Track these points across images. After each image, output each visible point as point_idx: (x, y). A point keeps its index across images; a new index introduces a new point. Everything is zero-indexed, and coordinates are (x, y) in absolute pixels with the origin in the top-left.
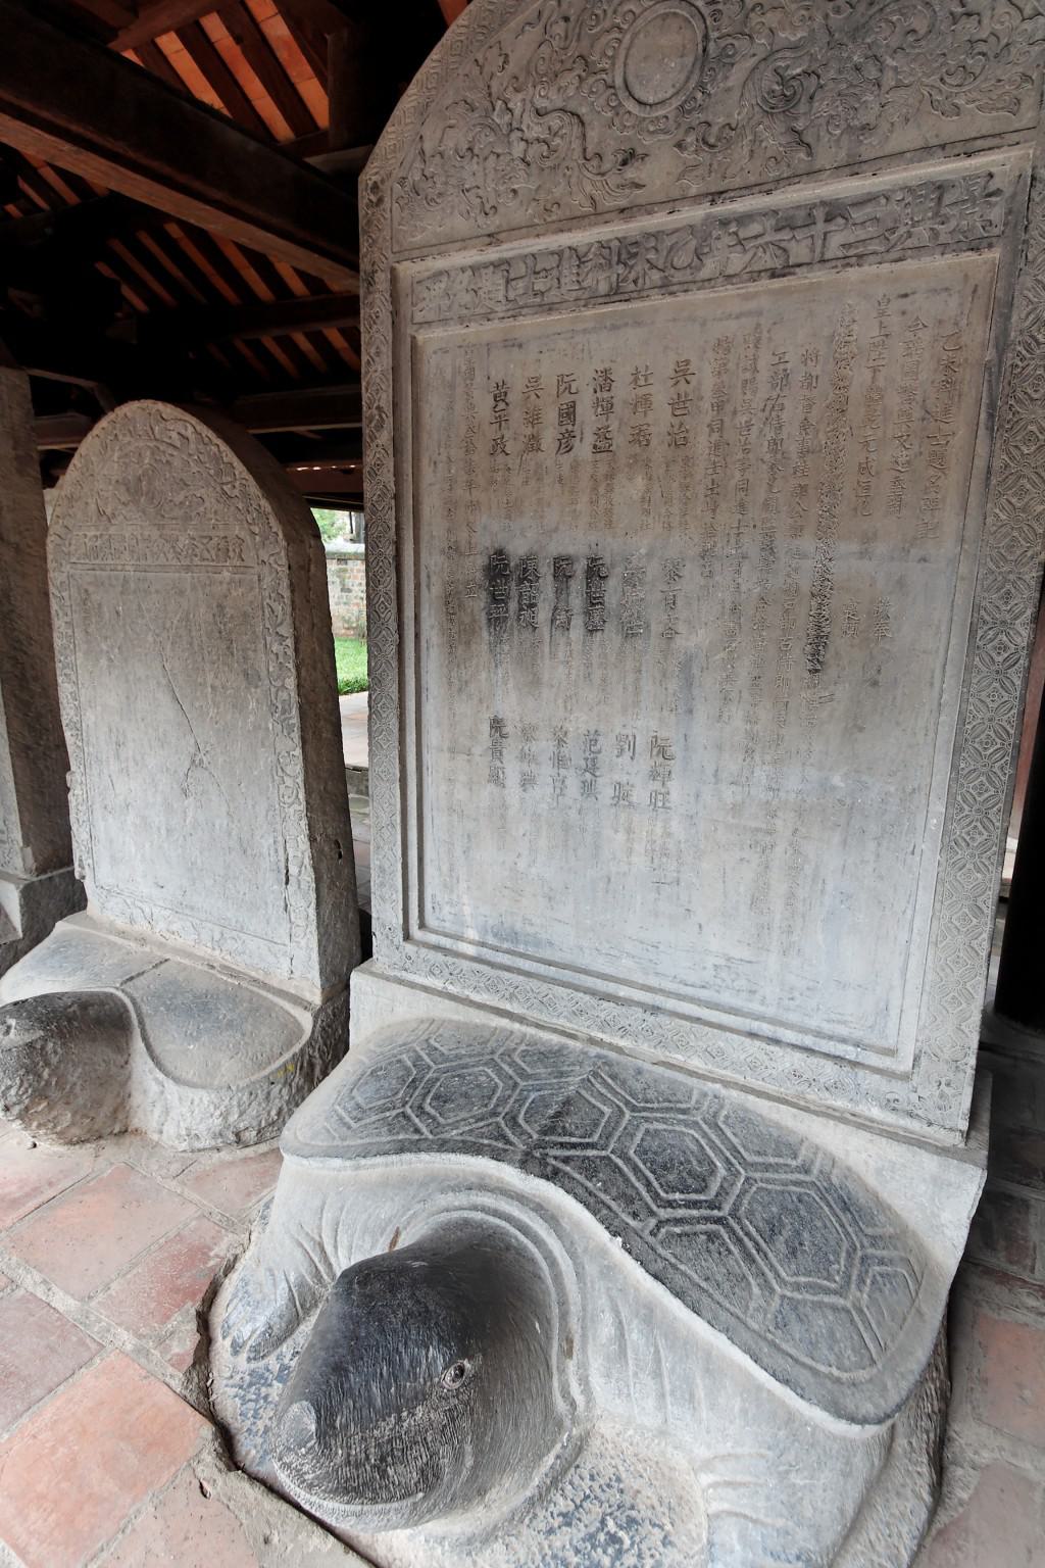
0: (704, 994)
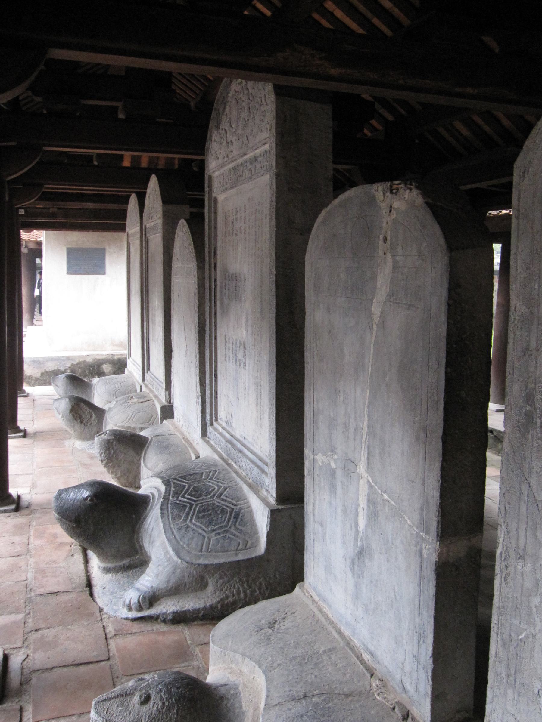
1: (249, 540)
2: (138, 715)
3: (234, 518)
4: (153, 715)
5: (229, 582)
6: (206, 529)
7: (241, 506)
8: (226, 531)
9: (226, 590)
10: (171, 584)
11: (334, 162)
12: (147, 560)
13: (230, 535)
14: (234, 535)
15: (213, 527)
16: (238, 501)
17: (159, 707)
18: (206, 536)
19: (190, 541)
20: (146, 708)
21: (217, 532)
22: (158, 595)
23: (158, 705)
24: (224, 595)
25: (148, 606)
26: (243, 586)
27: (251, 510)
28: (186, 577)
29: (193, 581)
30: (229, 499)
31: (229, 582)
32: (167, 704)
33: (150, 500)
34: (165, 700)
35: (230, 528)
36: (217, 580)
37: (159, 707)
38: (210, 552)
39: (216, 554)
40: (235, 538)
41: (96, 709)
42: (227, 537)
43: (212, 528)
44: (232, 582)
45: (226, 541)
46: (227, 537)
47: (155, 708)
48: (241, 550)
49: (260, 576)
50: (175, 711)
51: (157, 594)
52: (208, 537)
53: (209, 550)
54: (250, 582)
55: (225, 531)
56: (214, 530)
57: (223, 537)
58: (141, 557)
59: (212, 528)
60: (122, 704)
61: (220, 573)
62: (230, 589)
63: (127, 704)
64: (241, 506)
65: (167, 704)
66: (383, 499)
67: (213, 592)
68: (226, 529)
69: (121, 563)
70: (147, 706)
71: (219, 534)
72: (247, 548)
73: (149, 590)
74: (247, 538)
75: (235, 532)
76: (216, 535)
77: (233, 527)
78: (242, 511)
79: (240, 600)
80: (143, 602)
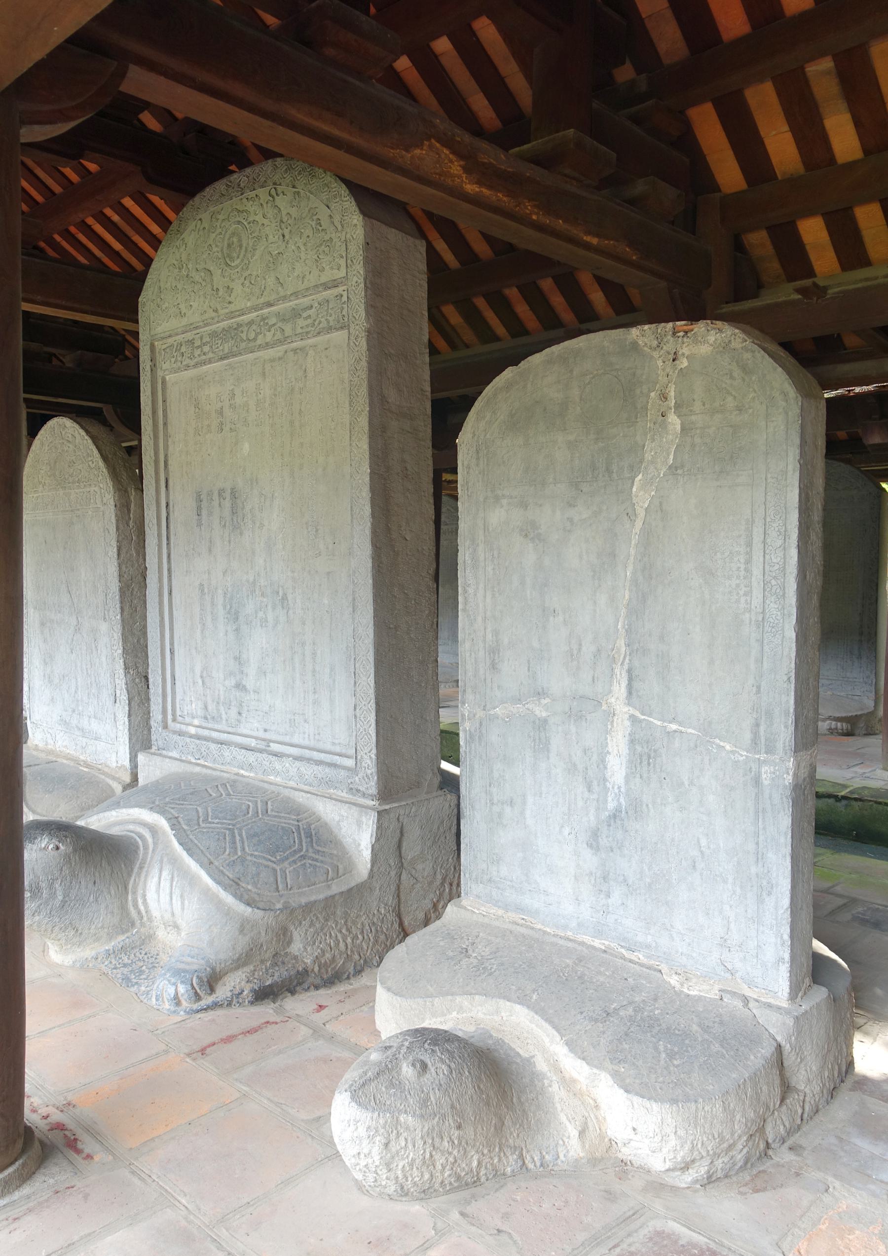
0: (287, 739)
1: (339, 865)
2: (423, 1092)
3: (307, 837)
4: (444, 1086)
5: (322, 930)
6: (273, 859)
7: (307, 820)
8: (303, 857)
9: (321, 943)
10: (239, 949)
11: (25, 392)
12: (152, 932)
13: (310, 862)
14: (316, 860)
15: (282, 853)
16: (298, 815)
17: (445, 1072)
18: (278, 868)
19: (256, 879)
20: (428, 1078)
21: (291, 860)
22: (220, 972)
23: (443, 1070)
24: (319, 950)
25: (209, 992)
26: (341, 932)
27: (326, 824)
28: (263, 934)
29: (272, 939)
30: (283, 815)
31: (322, 930)
32: (453, 1065)
33: (135, 840)
34: (447, 1061)
35: (307, 851)
36: (307, 930)
37: (445, 1072)
38: (290, 889)
39: (300, 890)
40: (318, 864)
41: (356, 1102)
42: (308, 865)
43: (281, 855)
44: (326, 929)
45: (309, 870)
46: (308, 865)
47: (441, 1075)
48: (333, 879)
49: (362, 914)
50: (467, 1073)
51: (218, 970)
52: (281, 869)
53: (289, 887)
54: (349, 924)
55: (301, 856)
56: (287, 858)
57: (302, 865)
58: (142, 930)
59: (281, 855)
60: (391, 1085)
61: (310, 918)
62: (326, 939)
63: (397, 1083)
64: (307, 820)
65: (453, 1065)
66: (669, 733)
67: (302, 949)
68: (302, 853)
69: (109, 946)
70: (428, 1076)
71: (295, 862)
72: (339, 875)
73: (205, 967)
74: (335, 862)
75: (314, 855)
76: (290, 864)
77: (311, 850)
78: (313, 826)
79: (341, 953)
80: (201, 986)
